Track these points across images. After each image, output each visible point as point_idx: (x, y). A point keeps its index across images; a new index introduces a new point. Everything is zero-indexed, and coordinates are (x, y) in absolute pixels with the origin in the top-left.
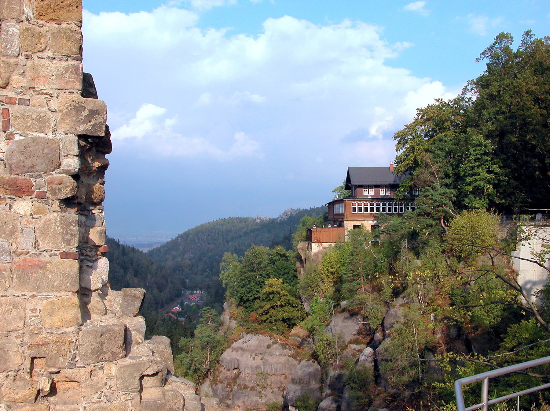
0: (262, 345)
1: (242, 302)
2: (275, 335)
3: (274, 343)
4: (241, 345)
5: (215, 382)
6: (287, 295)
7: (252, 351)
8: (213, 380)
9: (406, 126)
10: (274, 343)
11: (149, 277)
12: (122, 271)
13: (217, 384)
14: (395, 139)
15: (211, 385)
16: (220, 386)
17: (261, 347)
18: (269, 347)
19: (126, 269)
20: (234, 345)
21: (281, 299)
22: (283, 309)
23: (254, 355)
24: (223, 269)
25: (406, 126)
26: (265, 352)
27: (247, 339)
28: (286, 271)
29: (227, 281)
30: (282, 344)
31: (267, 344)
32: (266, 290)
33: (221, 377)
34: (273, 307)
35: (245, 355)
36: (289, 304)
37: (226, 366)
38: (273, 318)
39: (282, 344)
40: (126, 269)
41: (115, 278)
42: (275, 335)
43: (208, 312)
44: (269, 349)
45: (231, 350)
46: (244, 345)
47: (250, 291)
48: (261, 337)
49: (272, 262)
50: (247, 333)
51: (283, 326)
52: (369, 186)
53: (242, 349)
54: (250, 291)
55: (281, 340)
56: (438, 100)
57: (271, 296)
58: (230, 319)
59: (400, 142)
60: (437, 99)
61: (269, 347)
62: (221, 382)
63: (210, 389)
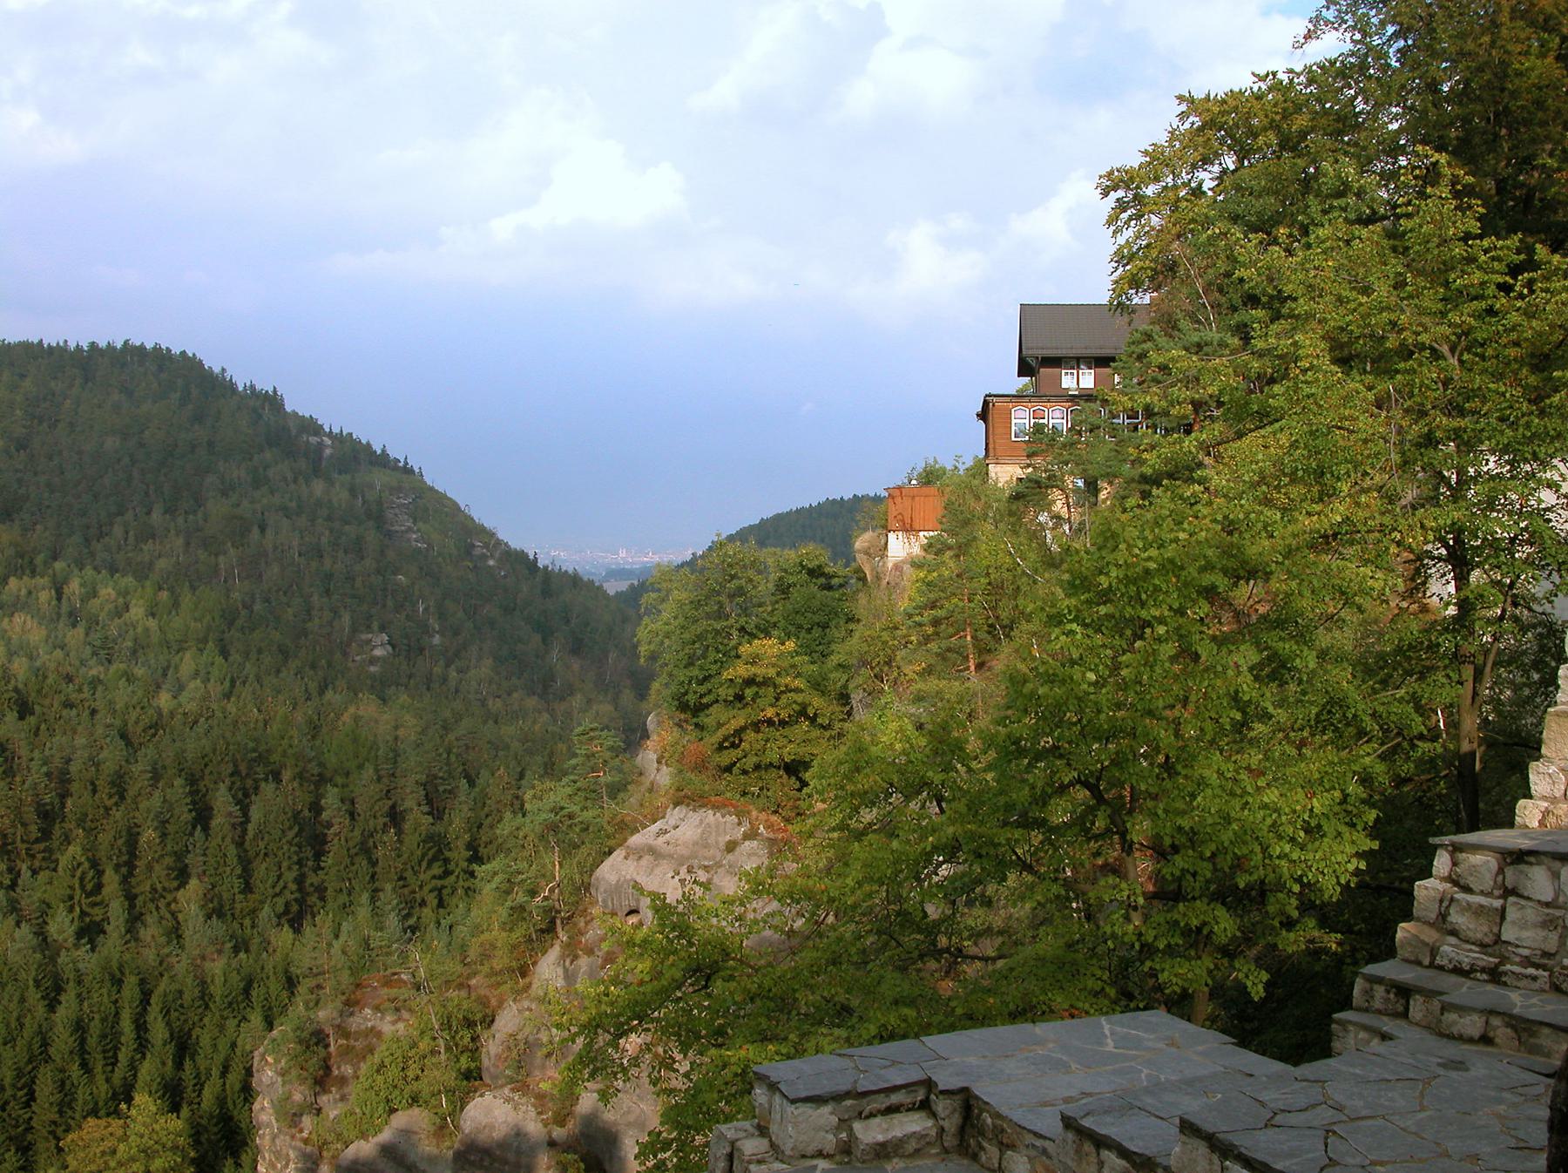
0: (711, 840)
1: (691, 709)
2: (754, 813)
3: (746, 837)
4: (651, 841)
5: (572, 951)
6: (797, 690)
7: (681, 861)
8: (568, 945)
9: (1146, 153)
10: (746, 837)
11: (612, 656)
12: (537, 638)
13: (576, 957)
14: (1105, 194)
15: (563, 957)
16: (584, 962)
17: (707, 846)
18: (731, 847)
19: (546, 633)
20: (635, 840)
21: (777, 699)
22: (787, 731)
23: (683, 870)
24: (648, 612)
25: (1146, 153)
26: (719, 865)
27: (672, 822)
28: (816, 618)
29: (652, 647)
30: (772, 841)
31: (728, 838)
32: (741, 670)
33: (591, 935)
34: (756, 726)
35: (657, 871)
36: (807, 717)
37: (604, 901)
38: (751, 761)
39: (772, 841)
40: (546, 633)
41: (515, 657)
42: (754, 813)
43: (592, 739)
44: (730, 857)
45: (624, 853)
46: (661, 840)
47: (706, 679)
48: (710, 816)
49: (783, 589)
50: (676, 805)
51: (781, 786)
52: (1076, 362)
53: (652, 851)
54: (706, 679)
55: (769, 827)
56: (1262, 79)
57: (749, 692)
58: (659, 762)
59: (1121, 206)
60: (1262, 73)
61: (731, 847)
62: (590, 952)
63: (560, 971)
